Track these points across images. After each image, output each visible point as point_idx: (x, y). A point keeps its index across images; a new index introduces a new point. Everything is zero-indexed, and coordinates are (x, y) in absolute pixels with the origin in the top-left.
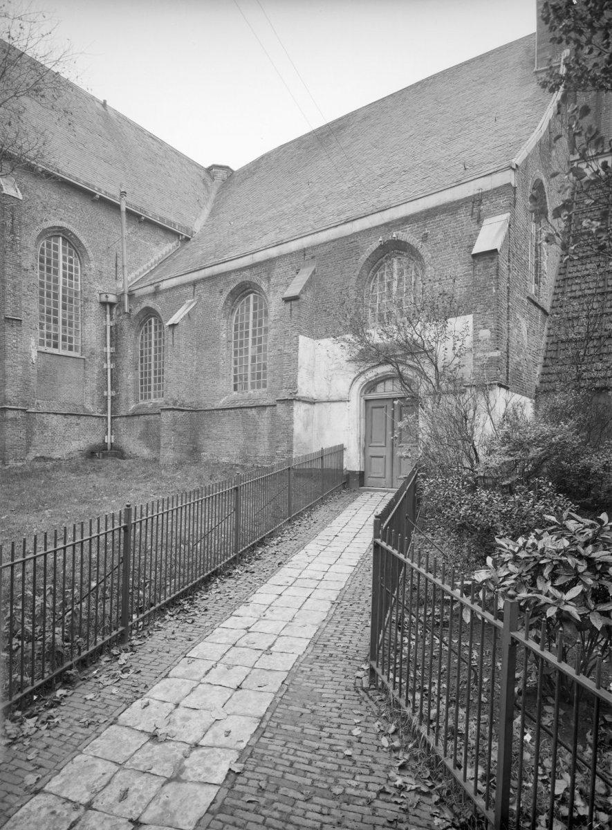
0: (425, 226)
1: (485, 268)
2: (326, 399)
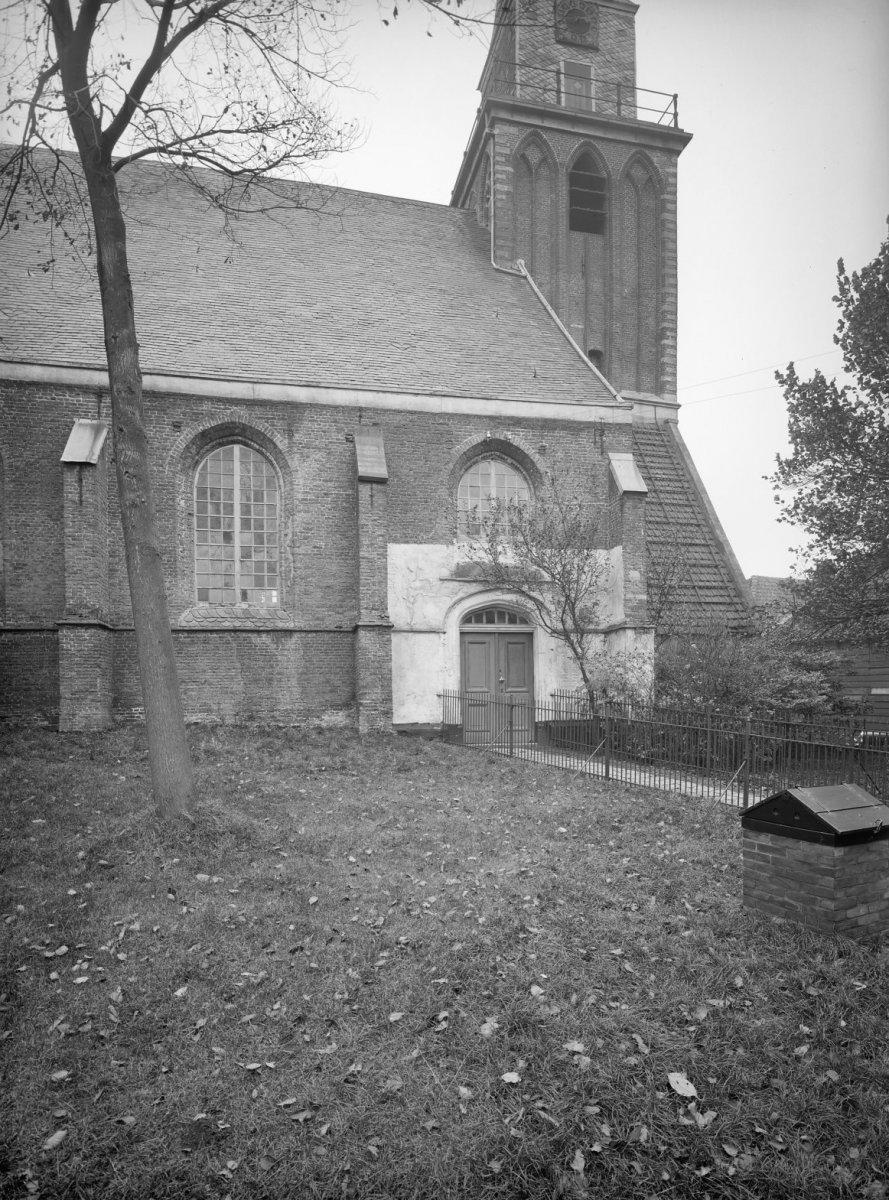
0: (542, 437)
1: (635, 507)
2: (406, 628)
